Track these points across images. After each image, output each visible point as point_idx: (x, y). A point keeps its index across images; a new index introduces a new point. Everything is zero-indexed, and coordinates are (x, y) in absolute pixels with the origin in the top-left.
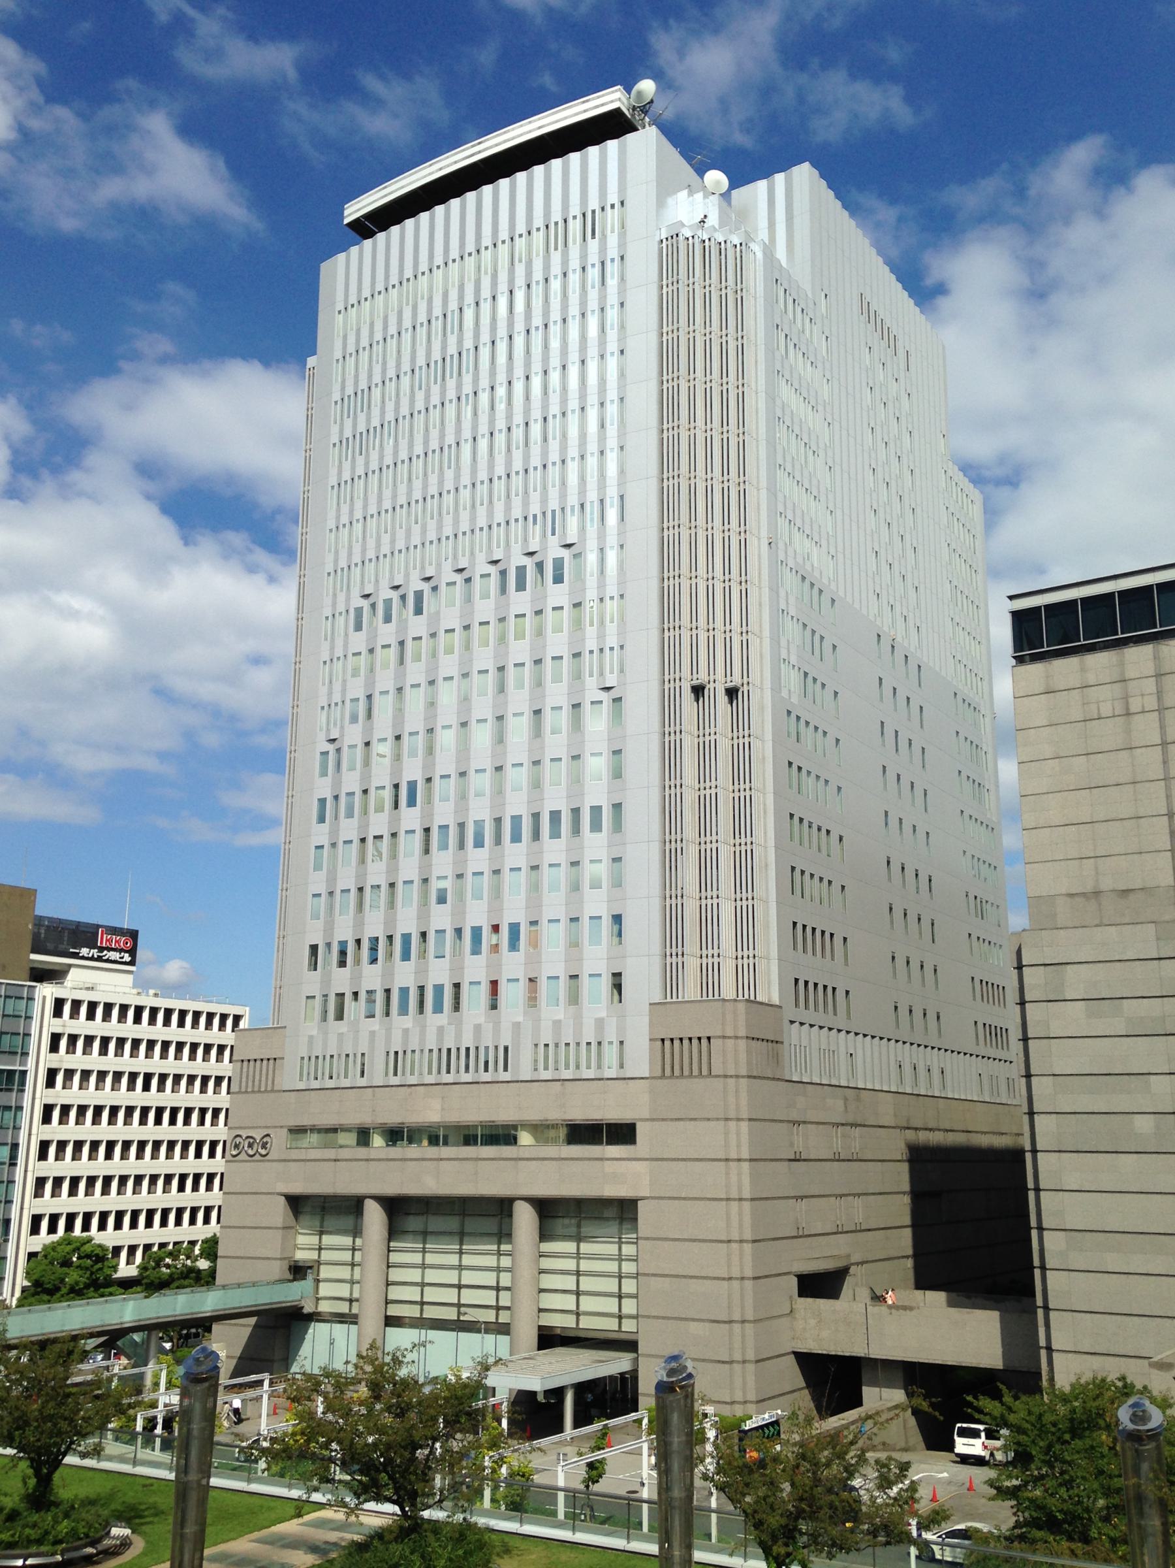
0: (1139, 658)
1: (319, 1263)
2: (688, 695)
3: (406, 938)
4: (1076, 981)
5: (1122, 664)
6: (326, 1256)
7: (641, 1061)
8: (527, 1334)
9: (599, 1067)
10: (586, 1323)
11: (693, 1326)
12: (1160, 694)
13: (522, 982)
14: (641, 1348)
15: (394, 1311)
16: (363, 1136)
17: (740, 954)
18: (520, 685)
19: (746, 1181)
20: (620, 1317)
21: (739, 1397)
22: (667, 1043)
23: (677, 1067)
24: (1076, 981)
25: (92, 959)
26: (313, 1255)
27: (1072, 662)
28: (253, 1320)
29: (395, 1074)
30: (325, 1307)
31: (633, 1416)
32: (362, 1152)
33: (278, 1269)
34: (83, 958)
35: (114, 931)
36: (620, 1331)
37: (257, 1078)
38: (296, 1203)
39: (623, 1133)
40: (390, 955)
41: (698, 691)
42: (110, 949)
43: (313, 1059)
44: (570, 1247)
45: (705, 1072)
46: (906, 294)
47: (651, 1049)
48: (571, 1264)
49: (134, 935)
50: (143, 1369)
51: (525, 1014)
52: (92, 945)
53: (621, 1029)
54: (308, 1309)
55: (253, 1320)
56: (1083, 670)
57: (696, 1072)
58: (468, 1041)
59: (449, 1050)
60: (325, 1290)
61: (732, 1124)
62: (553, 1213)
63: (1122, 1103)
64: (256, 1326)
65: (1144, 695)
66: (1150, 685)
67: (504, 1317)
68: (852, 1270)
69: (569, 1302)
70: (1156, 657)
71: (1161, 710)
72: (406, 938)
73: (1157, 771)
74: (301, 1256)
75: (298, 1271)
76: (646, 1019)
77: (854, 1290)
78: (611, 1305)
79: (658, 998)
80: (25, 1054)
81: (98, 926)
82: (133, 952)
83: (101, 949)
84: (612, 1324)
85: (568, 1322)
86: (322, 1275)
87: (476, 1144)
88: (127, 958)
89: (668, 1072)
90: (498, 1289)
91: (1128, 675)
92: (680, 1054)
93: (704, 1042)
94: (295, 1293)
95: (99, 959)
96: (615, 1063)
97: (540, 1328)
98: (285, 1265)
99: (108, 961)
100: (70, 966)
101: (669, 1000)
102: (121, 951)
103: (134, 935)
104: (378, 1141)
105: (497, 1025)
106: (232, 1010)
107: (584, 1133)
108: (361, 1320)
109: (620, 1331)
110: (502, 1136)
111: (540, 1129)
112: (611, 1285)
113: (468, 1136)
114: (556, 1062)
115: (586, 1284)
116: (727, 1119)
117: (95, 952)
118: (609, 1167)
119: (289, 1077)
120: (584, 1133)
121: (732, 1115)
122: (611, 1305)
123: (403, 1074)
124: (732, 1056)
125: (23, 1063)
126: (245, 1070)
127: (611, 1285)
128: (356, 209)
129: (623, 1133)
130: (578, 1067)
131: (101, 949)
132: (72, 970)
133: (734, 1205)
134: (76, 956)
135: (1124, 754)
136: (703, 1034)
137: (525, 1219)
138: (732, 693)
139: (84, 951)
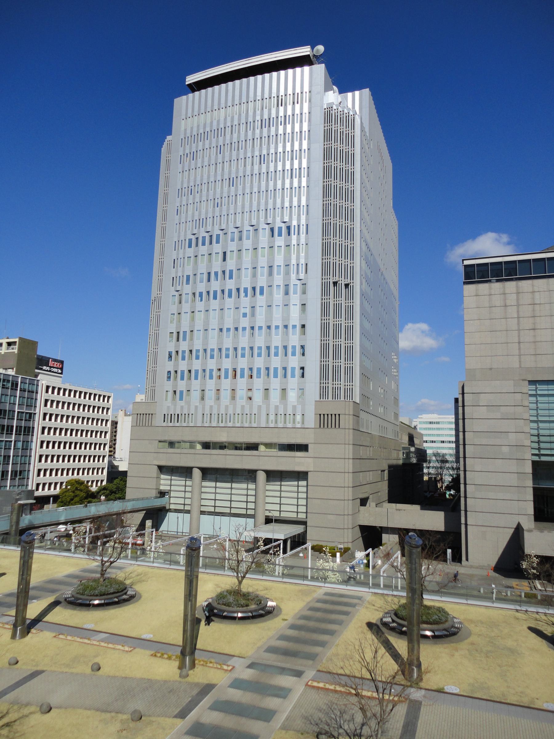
0: (511, 286)
1: (170, 490)
2: (332, 285)
3: (183, 372)
4: (484, 399)
5: (504, 288)
6: (173, 488)
7: (311, 421)
8: (261, 519)
9: (210, 422)
10: (283, 515)
11: (329, 516)
12: (518, 299)
13: (261, 390)
14: (308, 525)
15: (203, 509)
16: (192, 444)
17: (346, 384)
18: (262, 275)
19: (351, 466)
20: (280, 511)
21: (346, 541)
22: (139, 415)
23: (141, 423)
24: (484, 399)
25: (47, 371)
26: (168, 488)
27: (486, 285)
28: (145, 512)
29: (171, 422)
30: (172, 507)
31: (304, 547)
32: (192, 451)
33: (154, 493)
34: (44, 370)
35: (55, 360)
36: (297, 517)
37: (144, 421)
38: (162, 469)
39: (303, 448)
40: (176, 378)
41: (335, 283)
42: (54, 367)
43: (183, 415)
44: (213, 484)
45: (150, 425)
46: (385, 141)
47: (315, 417)
48: (278, 494)
49: (62, 362)
50: (144, 532)
51: (200, 403)
52: (47, 365)
53: (303, 409)
54: (167, 508)
55: (145, 512)
56: (490, 288)
57: (144, 425)
58: (239, 411)
59: (171, 415)
60: (172, 500)
61: (347, 446)
62: (274, 476)
63: (498, 442)
64: (145, 513)
65: (512, 299)
66: (515, 296)
67: (187, 508)
68: (371, 497)
69: (212, 503)
70: (517, 287)
71: (518, 305)
72: (183, 372)
73: (515, 327)
74: (162, 488)
75: (162, 494)
76: (314, 407)
77: (371, 504)
78: (244, 505)
79: (318, 399)
80: (35, 407)
81: (50, 358)
82: (62, 369)
83: (51, 367)
84: (295, 515)
85: (276, 514)
86: (172, 495)
87: (242, 450)
88: (60, 371)
89: (138, 425)
90: (185, 498)
91: (507, 292)
92: (327, 420)
93: (150, 415)
94: (159, 503)
95: (50, 371)
96: (208, 422)
97: (266, 516)
98: (157, 491)
99: (53, 372)
100: (39, 373)
101: (322, 400)
102: (58, 368)
103: (62, 362)
104: (199, 447)
105: (219, 406)
106: (107, 394)
107: (291, 447)
108: (191, 512)
109: (297, 517)
110: (253, 447)
111: (268, 445)
112: (294, 501)
113: (237, 447)
114: (242, 420)
115: (234, 498)
116: (345, 458)
117: (48, 368)
118: (297, 460)
119: (158, 421)
120: (291, 447)
121: (347, 442)
122: (244, 505)
123: (174, 422)
124: (347, 421)
125: (35, 410)
126: (139, 418)
127: (244, 498)
128: (191, 79)
129: (303, 448)
130: (250, 423)
131: (51, 367)
132: (40, 375)
133: (346, 474)
134: (41, 369)
135: (503, 320)
136: (337, 413)
137: (261, 476)
138: (347, 286)
139: (45, 368)
